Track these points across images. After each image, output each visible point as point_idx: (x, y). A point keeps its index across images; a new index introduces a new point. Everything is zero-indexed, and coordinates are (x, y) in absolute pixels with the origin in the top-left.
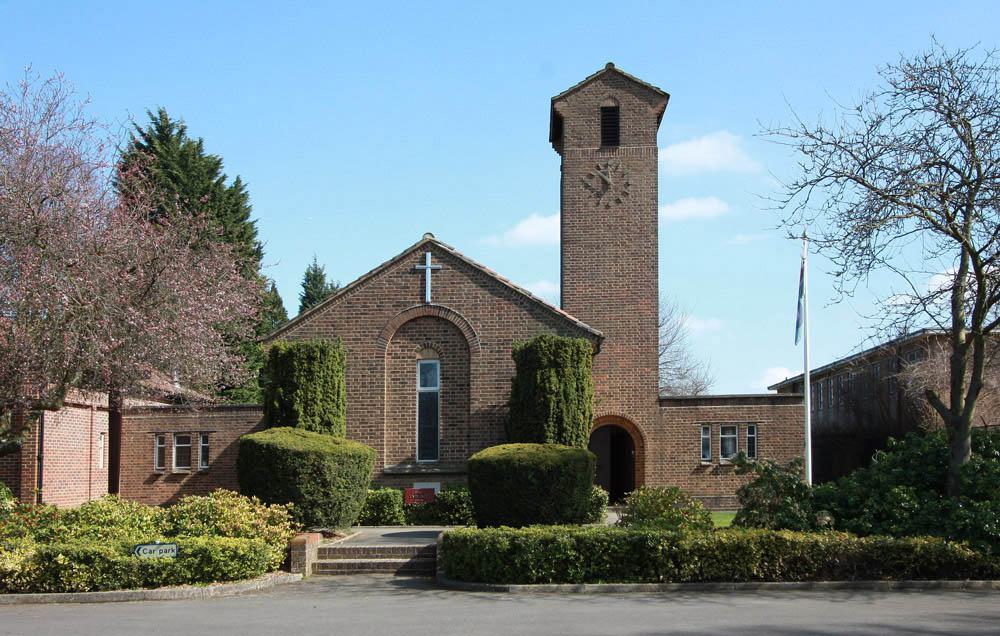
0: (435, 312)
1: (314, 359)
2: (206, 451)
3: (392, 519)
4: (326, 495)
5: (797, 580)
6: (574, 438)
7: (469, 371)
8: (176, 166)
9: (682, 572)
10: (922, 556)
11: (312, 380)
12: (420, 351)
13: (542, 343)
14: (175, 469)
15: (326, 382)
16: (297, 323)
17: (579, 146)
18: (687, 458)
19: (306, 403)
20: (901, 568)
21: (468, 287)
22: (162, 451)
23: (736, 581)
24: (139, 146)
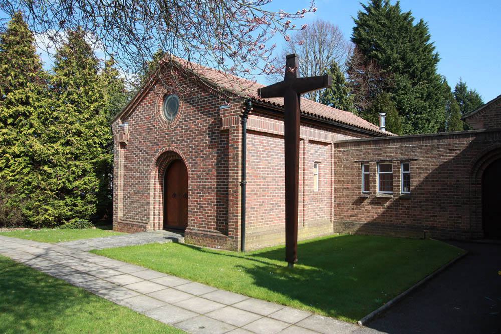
2: (407, 178)
14: (379, 193)
22: (367, 177)
24: (363, 14)
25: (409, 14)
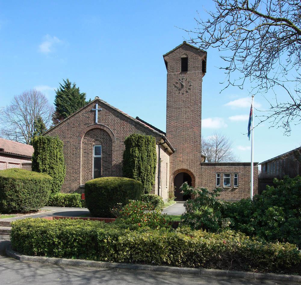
0: (99, 127)
1: (45, 143)
3: (76, 205)
4: (18, 196)
5: (192, 267)
6: (146, 175)
7: (112, 149)
8: (70, 95)
9: (119, 256)
10: (280, 258)
11: (44, 151)
12: (94, 142)
13: (133, 137)
15: (50, 152)
16: (50, 131)
17: (173, 72)
18: (211, 185)
19: (42, 160)
20: (265, 264)
21: (112, 117)
23: (154, 264)
25: (84, 95)
